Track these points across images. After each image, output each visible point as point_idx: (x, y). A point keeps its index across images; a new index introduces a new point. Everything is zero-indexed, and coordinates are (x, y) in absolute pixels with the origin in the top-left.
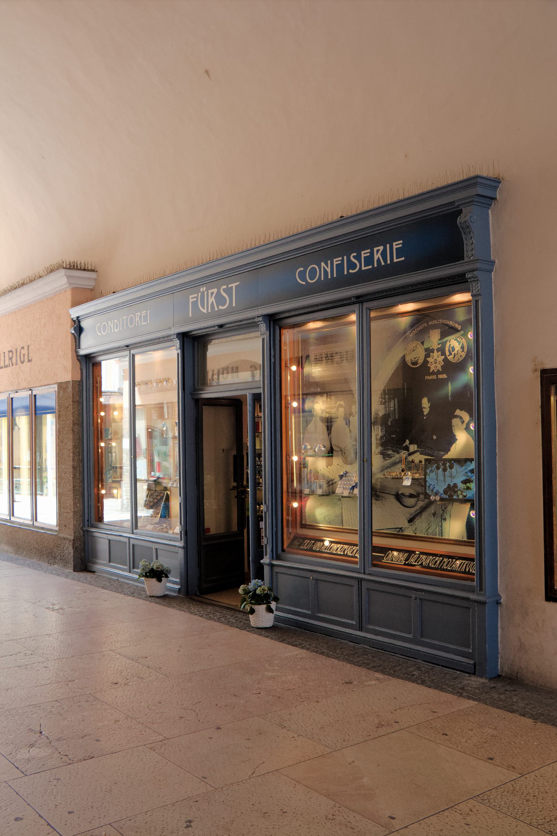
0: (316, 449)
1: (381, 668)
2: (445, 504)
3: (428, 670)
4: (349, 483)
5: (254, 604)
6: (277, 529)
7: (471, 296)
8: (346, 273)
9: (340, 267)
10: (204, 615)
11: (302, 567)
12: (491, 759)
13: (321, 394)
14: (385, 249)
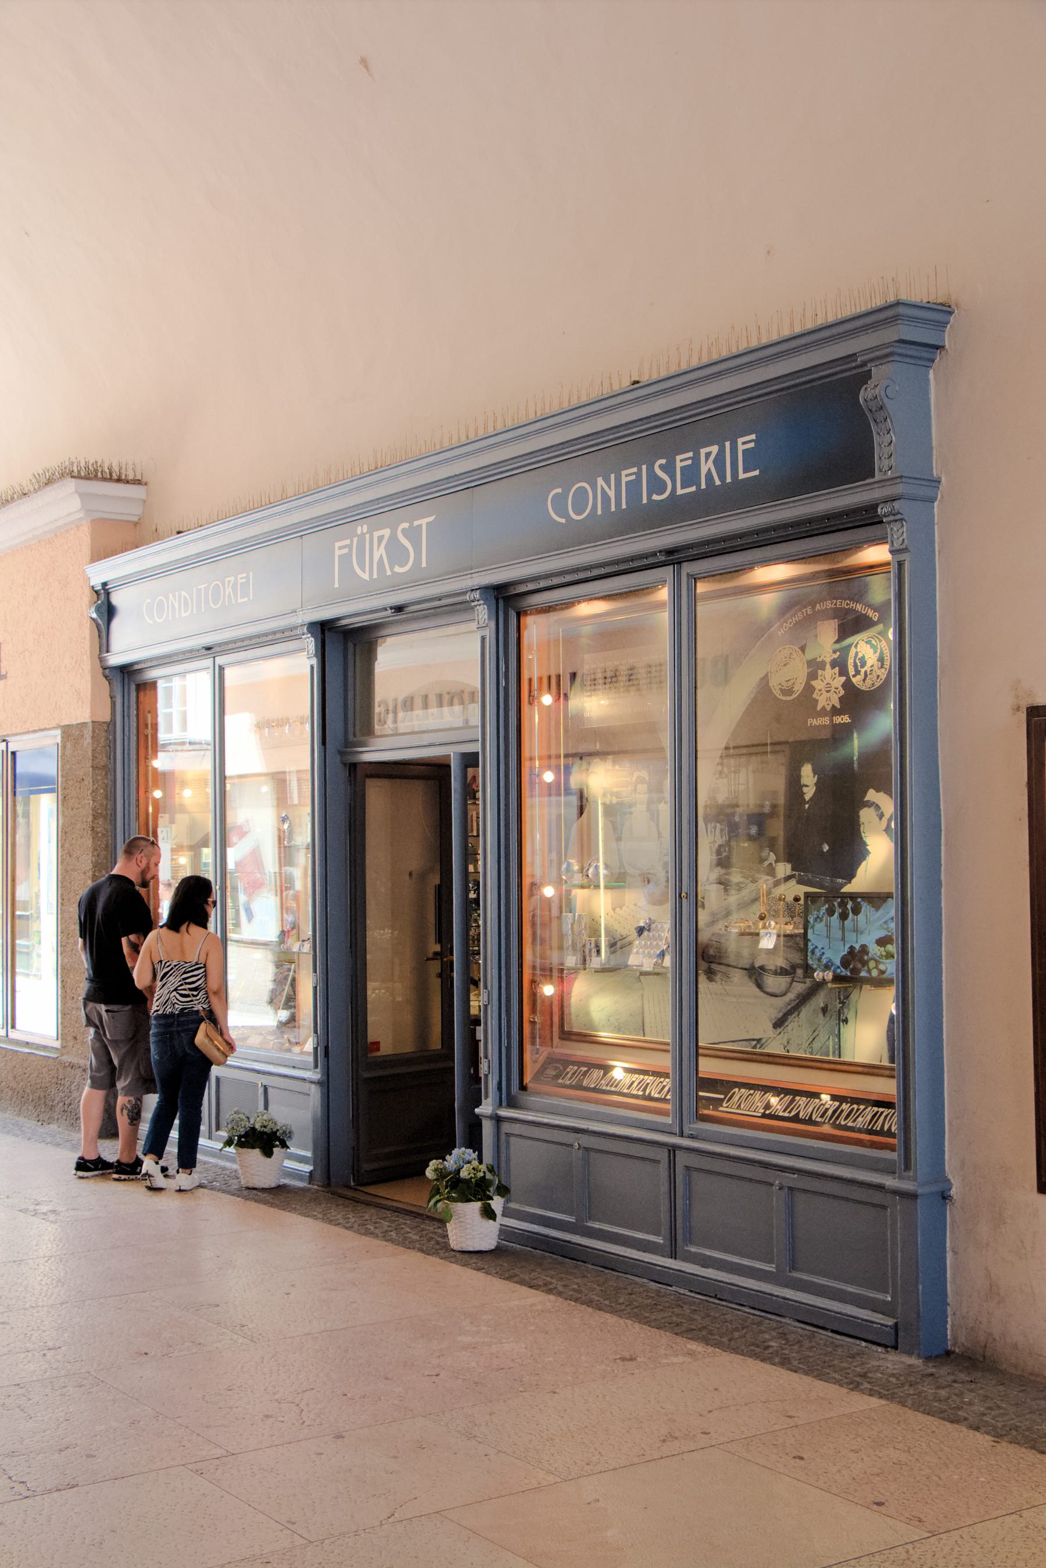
0: (590, 871)
1: (704, 1333)
2: (846, 988)
3: (801, 1339)
4: (655, 943)
5: (454, 1200)
6: (509, 1043)
7: (891, 552)
8: (645, 501)
9: (634, 487)
10: (356, 1226)
11: (557, 1122)
12: (879, 1504)
13: (602, 754)
14: (722, 451)
